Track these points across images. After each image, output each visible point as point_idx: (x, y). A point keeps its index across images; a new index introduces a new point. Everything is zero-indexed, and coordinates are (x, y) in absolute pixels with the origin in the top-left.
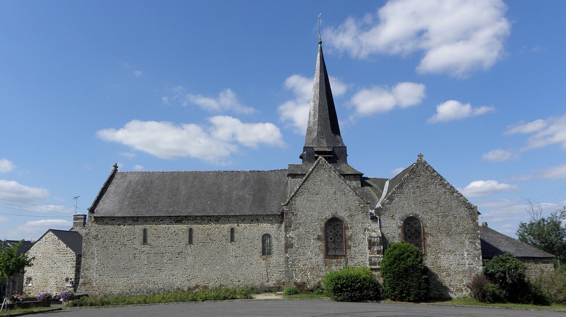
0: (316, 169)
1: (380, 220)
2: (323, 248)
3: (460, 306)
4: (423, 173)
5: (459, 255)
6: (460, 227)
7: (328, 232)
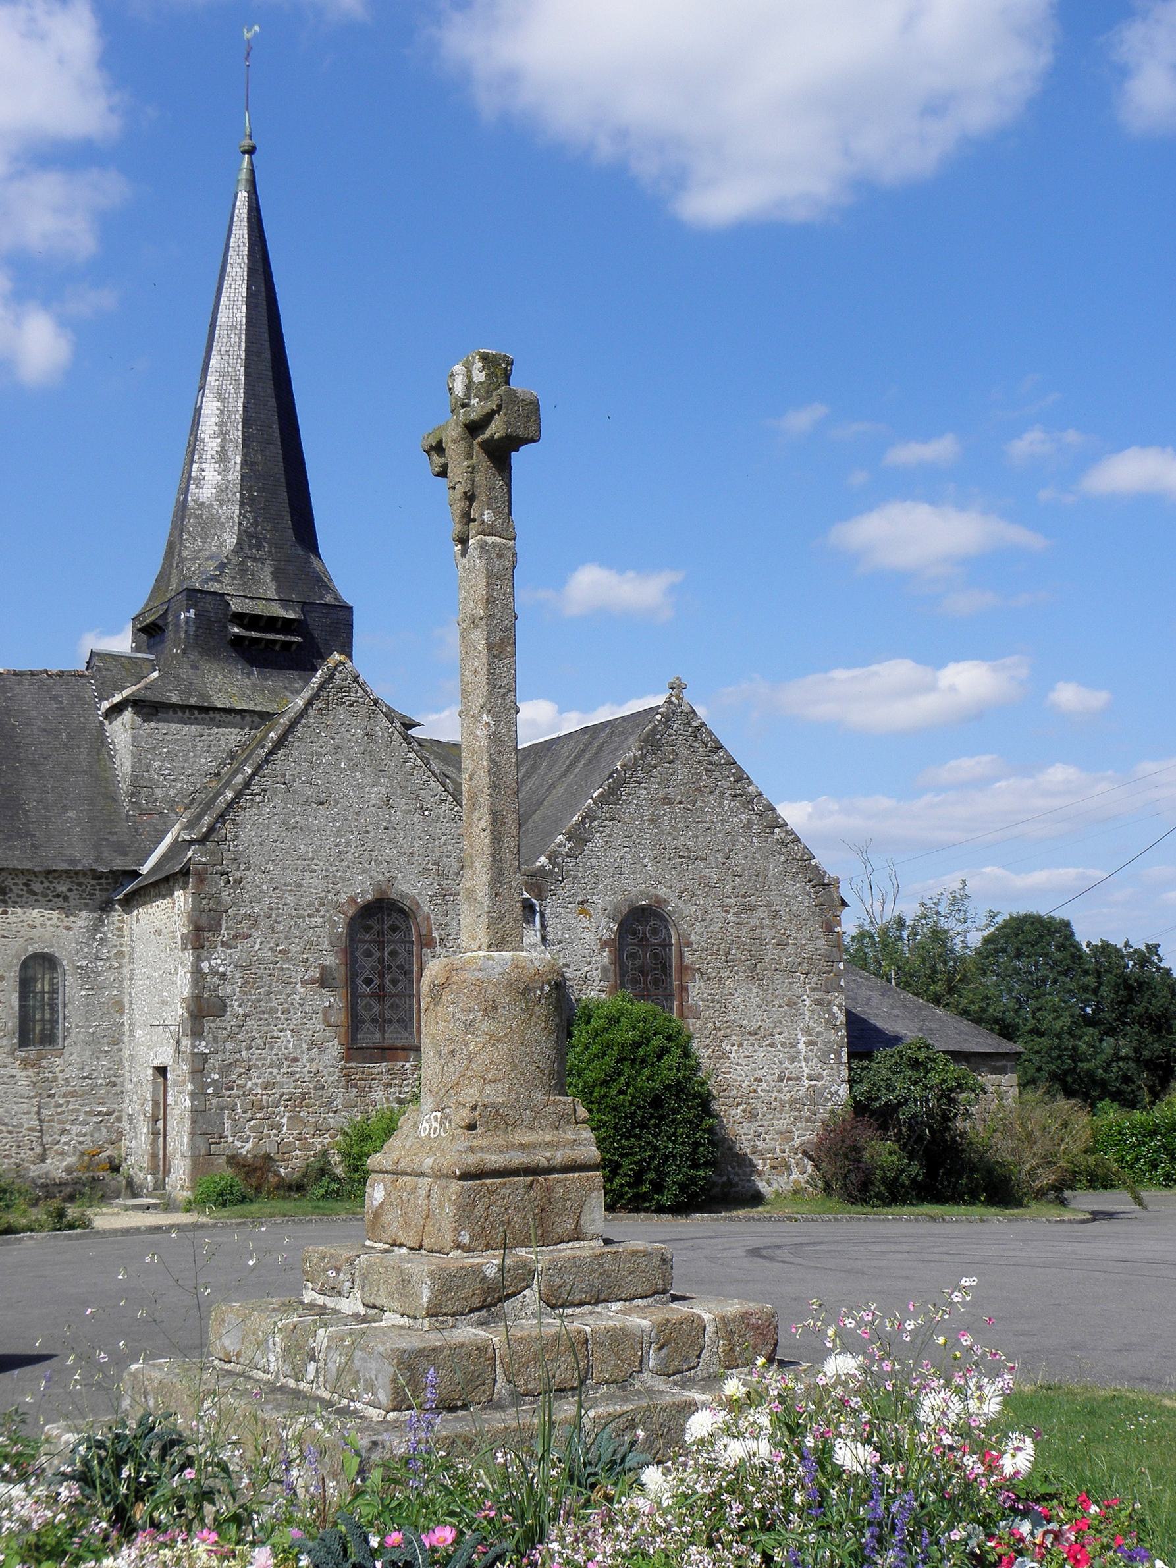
0: (318, 704)
1: (542, 916)
2: (340, 1018)
3: (806, 1220)
4: (683, 751)
5: (783, 1044)
6: (790, 949)
7: (358, 953)
